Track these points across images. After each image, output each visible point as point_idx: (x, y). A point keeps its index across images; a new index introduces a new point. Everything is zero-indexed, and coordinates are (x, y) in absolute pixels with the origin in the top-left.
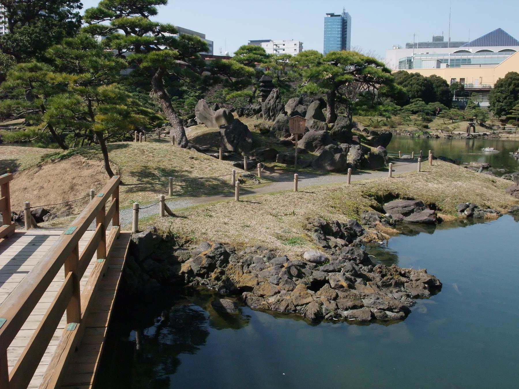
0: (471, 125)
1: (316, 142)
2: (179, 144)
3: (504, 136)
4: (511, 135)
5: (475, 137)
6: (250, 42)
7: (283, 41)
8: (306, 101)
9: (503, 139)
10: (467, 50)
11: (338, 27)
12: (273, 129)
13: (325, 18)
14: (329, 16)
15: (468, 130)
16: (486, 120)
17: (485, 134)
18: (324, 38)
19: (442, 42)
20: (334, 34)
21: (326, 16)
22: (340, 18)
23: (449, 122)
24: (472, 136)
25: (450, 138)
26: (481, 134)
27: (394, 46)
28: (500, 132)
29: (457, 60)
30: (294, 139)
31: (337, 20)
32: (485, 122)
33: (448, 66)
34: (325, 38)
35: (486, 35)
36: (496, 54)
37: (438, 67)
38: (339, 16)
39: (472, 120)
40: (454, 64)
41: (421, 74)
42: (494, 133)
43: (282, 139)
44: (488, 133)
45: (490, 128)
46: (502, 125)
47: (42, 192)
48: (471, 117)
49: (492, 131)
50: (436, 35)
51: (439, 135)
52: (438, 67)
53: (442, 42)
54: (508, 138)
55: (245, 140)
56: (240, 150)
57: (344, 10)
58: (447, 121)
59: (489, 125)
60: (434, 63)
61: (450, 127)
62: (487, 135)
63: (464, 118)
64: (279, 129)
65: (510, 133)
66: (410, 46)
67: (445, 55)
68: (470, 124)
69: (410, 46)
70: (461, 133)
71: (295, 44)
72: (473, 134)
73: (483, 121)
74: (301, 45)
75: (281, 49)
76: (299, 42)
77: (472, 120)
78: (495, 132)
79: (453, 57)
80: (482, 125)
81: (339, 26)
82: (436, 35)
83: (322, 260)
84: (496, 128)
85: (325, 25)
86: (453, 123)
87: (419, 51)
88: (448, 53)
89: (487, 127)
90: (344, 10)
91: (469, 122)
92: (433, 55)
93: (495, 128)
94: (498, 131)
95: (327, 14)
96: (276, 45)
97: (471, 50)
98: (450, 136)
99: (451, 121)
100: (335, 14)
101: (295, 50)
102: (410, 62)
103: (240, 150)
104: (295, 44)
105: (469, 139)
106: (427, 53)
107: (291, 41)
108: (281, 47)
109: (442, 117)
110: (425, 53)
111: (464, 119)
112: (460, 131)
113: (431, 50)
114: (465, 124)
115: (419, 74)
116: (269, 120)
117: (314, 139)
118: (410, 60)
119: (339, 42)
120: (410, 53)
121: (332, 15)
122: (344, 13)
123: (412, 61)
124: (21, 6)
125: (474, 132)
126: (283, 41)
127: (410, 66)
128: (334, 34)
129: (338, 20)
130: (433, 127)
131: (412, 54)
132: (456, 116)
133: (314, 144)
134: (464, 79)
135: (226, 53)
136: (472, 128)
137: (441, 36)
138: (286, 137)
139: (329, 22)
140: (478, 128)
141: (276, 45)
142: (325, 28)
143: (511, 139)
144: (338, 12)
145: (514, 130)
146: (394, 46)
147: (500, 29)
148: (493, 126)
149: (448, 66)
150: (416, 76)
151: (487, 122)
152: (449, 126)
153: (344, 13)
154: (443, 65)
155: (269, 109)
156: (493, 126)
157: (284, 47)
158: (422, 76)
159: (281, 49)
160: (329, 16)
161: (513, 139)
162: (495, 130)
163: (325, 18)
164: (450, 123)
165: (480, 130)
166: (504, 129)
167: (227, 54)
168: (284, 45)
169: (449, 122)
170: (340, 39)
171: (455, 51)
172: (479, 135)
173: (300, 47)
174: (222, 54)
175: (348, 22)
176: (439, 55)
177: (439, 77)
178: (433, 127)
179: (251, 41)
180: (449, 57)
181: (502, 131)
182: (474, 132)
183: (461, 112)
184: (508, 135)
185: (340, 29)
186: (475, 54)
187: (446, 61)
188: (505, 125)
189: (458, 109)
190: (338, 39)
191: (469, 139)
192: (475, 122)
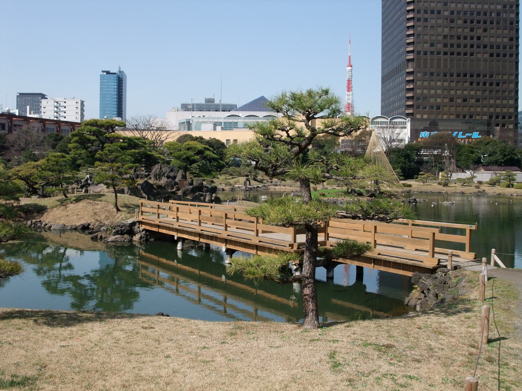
0: (248, 180)
1: (189, 191)
2: (127, 193)
3: (272, 188)
4: (277, 187)
5: (251, 189)
6: (19, 94)
7: (65, 99)
8: (174, 170)
9: (271, 190)
10: (238, 114)
11: (114, 85)
12: (165, 185)
13: (101, 75)
14: (105, 73)
15: (245, 184)
16: (257, 175)
17: (258, 187)
18: (100, 95)
19: (213, 104)
20: (110, 91)
21: (102, 73)
22: (115, 75)
23: (230, 177)
24: (249, 188)
25: (233, 190)
26: (255, 186)
27: (173, 108)
28: (269, 185)
29: (229, 123)
30: (176, 191)
31: (113, 78)
32: (257, 177)
33: (222, 129)
34: (100, 95)
35: (252, 101)
36: (261, 119)
37: (215, 129)
38: (115, 74)
39: (247, 176)
40: (228, 127)
41: (204, 137)
42: (264, 186)
43: (170, 191)
44: (260, 186)
45: (261, 181)
46: (270, 179)
47: (79, 217)
48: (246, 173)
49: (263, 184)
50: (208, 97)
51: (224, 188)
52: (215, 129)
53: (213, 104)
54: (275, 189)
55: (153, 191)
56: (150, 196)
57: (120, 68)
58: (228, 177)
59: (260, 179)
60: (211, 126)
61: (232, 181)
62: (260, 187)
63: (240, 174)
64: (168, 185)
65: (276, 185)
66: (185, 107)
67: (219, 118)
68: (246, 179)
69: (185, 107)
70: (240, 186)
71: (77, 102)
72: (249, 187)
73: (256, 176)
74: (83, 103)
75: (62, 106)
76: (81, 101)
77: (247, 176)
78: (265, 185)
79: (226, 121)
80: (255, 180)
81: (114, 84)
82: (207, 97)
83: (411, 63)
84: (266, 182)
85: (101, 82)
86: (232, 178)
87: (197, 114)
88: (222, 116)
89: (259, 181)
90: (120, 68)
91: (245, 178)
92: (209, 118)
93: (265, 181)
94: (267, 184)
95: (103, 72)
96: (57, 102)
97: (240, 115)
98: (233, 189)
99: (231, 177)
100: (111, 72)
101: (77, 108)
102: (188, 124)
103: (150, 196)
104: (77, 102)
105: (247, 190)
106: (204, 116)
107: (72, 99)
108: (62, 104)
109: (224, 173)
110: (202, 116)
111: (240, 175)
112: (239, 184)
113: (207, 114)
114: (243, 179)
115: (202, 137)
116: (157, 180)
117: (187, 190)
118: (189, 122)
119: (116, 99)
120: (187, 115)
121: (108, 73)
122: (120, 72)
123: (191, 122)
124: (110, 144)
125: (250, 185)
126: (65, 99)
127: (189, 127)
128: (110, 91)
129: (114, 78)
130: (217, 182)
131: (191, 116)
132: (234, 173)
133: (187, 193)
134: (237, 140)
135: (7, 109)
136: (248, 182)
137: (213, 98)
138: (171, 190)
139: (104, 79)
140: (252, 182)
141: (57, 102)
142: (101, 85)
143: (277, 190)
144: (114, 70)
145: (279, 183)
146: (173, 108)
147: (263, 96)
148: (263, 180)
149: (222, 129)
150: (200, 139)
151: (258, 177)
152: (230, 181)
153: (120, 72)
154: (219, 128)
155: (157, 174)
156: (263, 180)
157: (65, 104)
158: (205, 139)
159: (62, 106)
160: (105, 73)
161: (279, 190)
162: (265, 183)
163: (101, 75)
164: (230, 179)
165: (255, 184)
166: (272, 182)
167: (7, 111)
168: (65, 102)
169: (230, 177)
170: (116, 96)
171: (228, 115)
172: (254, 188)
173: (81, 105)
174: (3, 110)
175: (124, 80)
176: (214, 118)
177: (219, 140)
178: (217, 182)
179: (20, 94)
180: (223, 121)
181: (270, 184)
182: (250, 185)
183: (237, 169)
184: (275, 187)
185: (116, 87)
186: (244, 119)
187: (220, 124)
188: (272, 179)
189: (235, 166)
190: (114, 96)
191: (247, 190)
192: (250, 177)
